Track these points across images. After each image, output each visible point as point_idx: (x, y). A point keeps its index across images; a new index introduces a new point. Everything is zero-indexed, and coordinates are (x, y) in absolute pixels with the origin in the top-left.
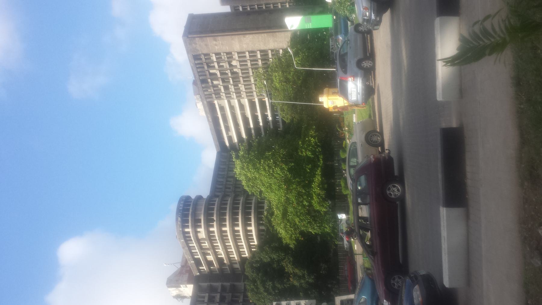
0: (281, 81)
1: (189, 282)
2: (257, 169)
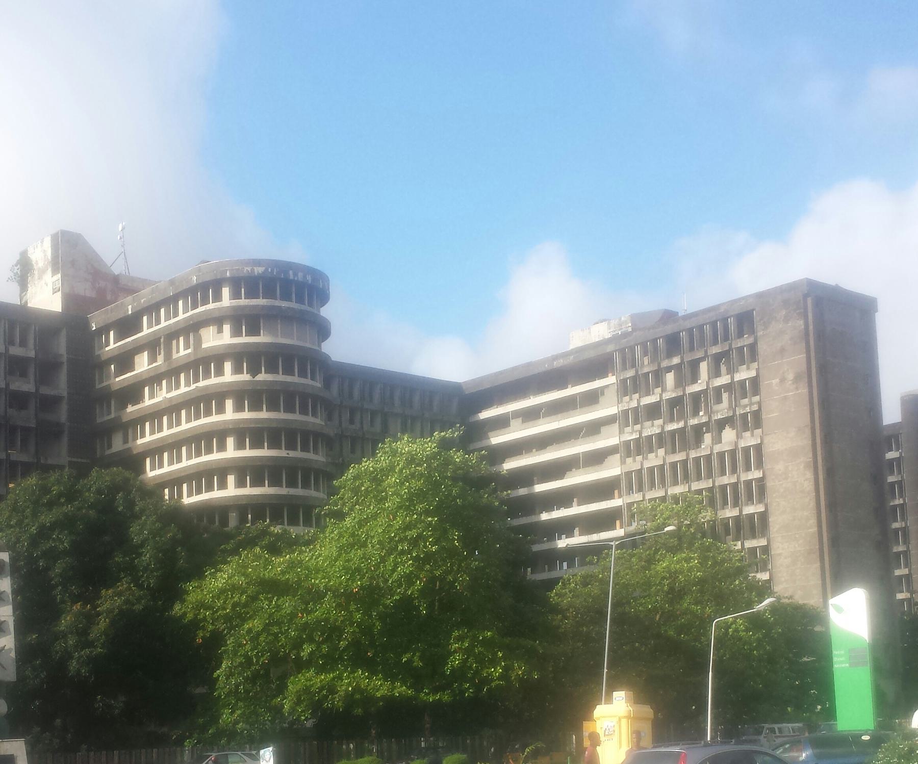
0: (673, 575)
1: (70, 300)
2: (408, 505)
